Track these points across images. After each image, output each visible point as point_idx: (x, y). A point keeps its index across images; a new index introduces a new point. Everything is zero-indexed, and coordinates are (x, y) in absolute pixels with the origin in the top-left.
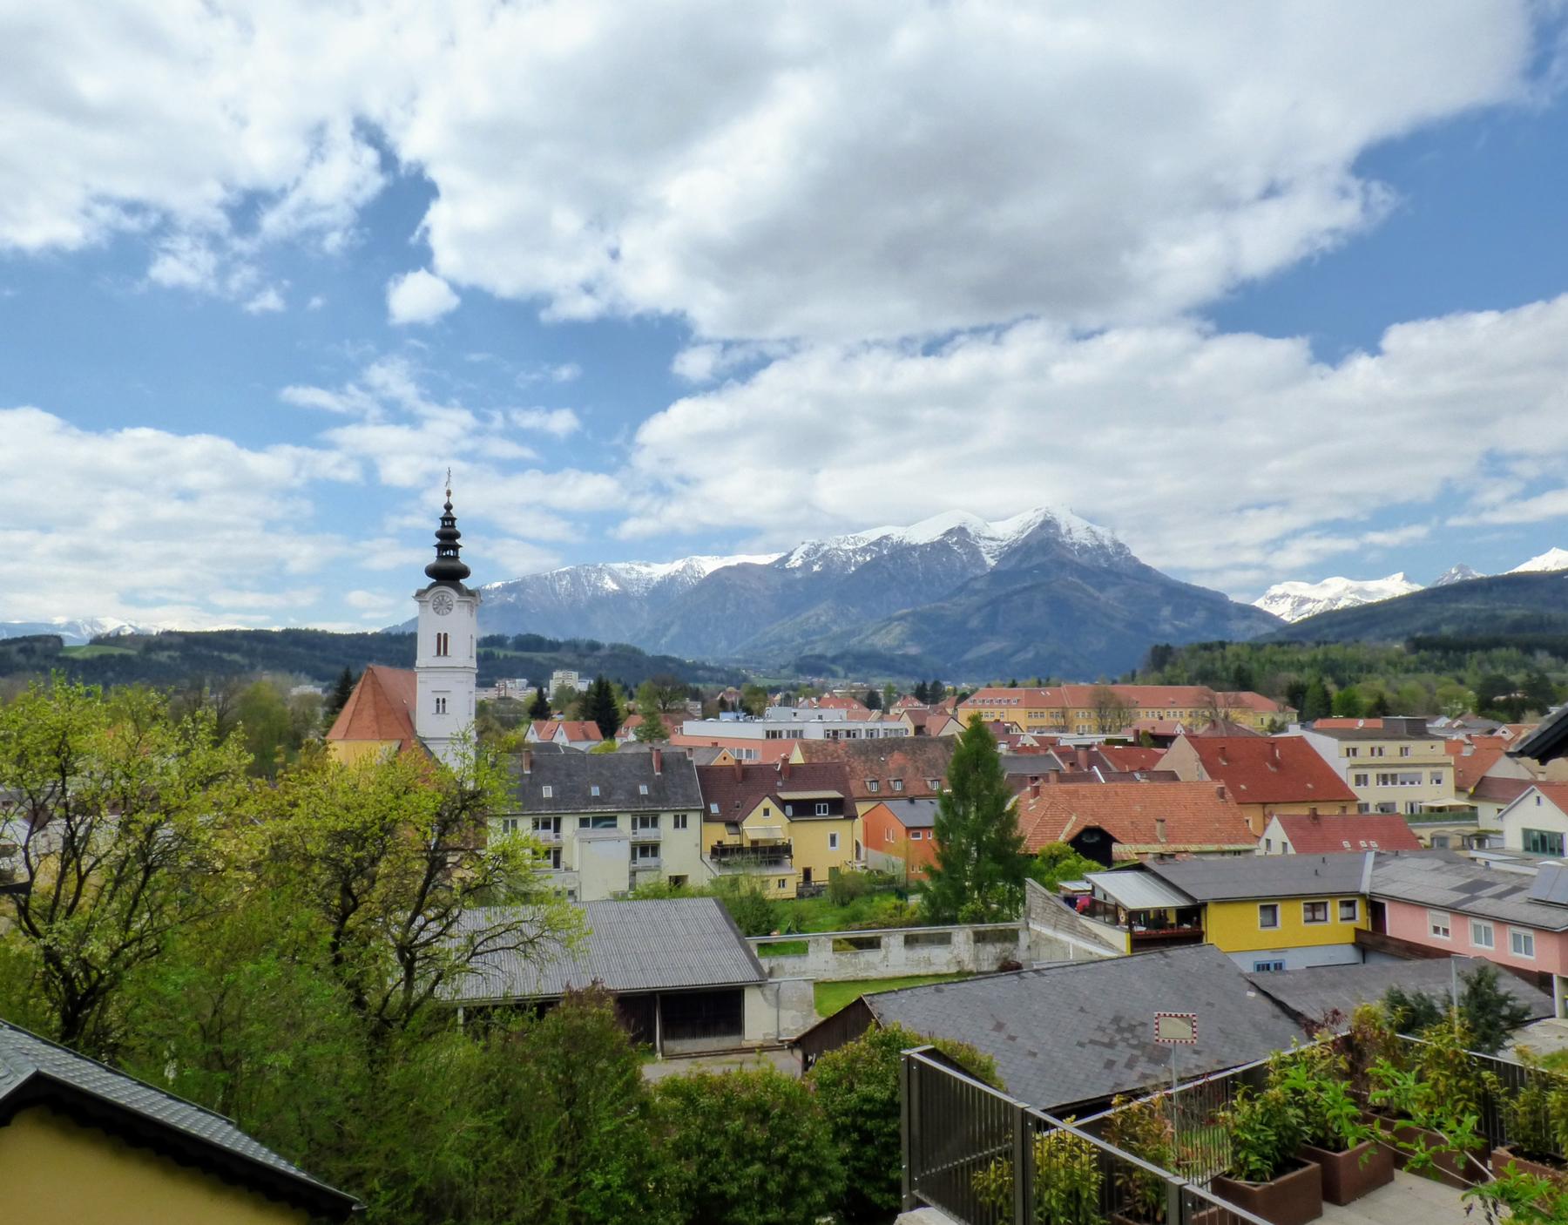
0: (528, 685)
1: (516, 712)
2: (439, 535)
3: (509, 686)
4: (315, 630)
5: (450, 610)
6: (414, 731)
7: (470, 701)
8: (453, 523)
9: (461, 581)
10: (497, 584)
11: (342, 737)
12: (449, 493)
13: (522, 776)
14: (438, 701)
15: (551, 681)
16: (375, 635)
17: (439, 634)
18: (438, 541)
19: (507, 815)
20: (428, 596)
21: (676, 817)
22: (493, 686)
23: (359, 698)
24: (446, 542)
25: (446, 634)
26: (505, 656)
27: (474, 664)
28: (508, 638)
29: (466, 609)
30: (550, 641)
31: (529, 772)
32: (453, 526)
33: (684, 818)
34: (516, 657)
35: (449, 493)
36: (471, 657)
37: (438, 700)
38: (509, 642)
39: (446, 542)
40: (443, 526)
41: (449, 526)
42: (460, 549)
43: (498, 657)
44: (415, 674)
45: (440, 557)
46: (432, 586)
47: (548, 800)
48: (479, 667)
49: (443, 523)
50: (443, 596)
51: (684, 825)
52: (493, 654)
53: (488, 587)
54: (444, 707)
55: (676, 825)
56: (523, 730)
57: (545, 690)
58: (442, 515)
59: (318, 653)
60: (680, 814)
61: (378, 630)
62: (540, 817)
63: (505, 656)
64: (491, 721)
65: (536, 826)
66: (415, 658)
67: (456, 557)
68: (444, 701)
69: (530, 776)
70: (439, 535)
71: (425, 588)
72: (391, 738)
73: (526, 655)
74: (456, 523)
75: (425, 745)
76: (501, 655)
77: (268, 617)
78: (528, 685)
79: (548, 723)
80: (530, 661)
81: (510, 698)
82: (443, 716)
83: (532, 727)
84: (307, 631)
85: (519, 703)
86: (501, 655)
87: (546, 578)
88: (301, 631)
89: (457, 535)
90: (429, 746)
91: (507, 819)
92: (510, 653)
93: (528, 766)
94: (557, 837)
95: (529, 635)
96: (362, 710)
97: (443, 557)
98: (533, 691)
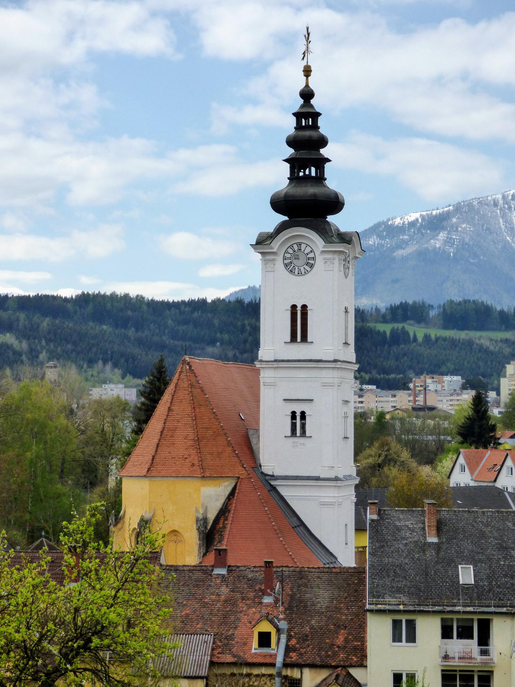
0: (464, 387)
1: (437, 431)
2: (291, 142)
3: (432, 387)
4: (126, 296)
5: (312, 266)
6: (256, 465)
7: (346, 417)
8: (315, 122)
9: (330, 218)
10: (413, 217)
11: (144, 472)
12: (307, 72)
13: (424, 546)
14: (293, 415)
15: (503, 380)
16: (217, 302)
17: (294, 307)
18: (290, 152)
19: (399, 612)
20: (276, 245)
21: (396, 624)
22: (405, 387)
23: (170, 409)
24: (304, 154)
25: (304, 307)
26: (427, 337)
27: (350, 354)
28: (431, 307)
29: (337, 262)
30: (502, 313)
31: (435, 540)
32: (315, 127)
33: (411, 625)
34: (445, 339)
35: (307, 72)
36: (346, 343)
37: (294, 414)
38: (432, 313)
39: (304, 154)
40: (299, 127)
41: (307, 127)
42: (327, 165)
43: (415, 339)
44: (257, 371)
45: (293, 178)
46: (282, 228)
47: (467, 588)
48: (358, 361)
49: (299, 122)
50: (299, 244)
51: (412, 638)
52: (405, 333)
53: (398, 221)
54: (303, 426)
55: (397, 638)
56: (446, 463)
57: (492, 395)
58: (296, 109)
59: (131, 332)
60: (404, 618)
61: (223, 294)
62: (455, 617)
63: (427, 337)
64: (395, 446)
65: (446, 633)
66: (256, 344)
67: (320, 179)
68: (303, 415)
69: (438, 547)
70: (291, 142)
71: (271, 229)
72: (219, 477)
73: (463, 335)
74: (321, 121)
75: (274, 488)
76: (420, 337)
77: (47, 276)
78: (464, 387)
79: (489, 453)
80: (470, 343)
81: (432, 409)
82: (302, 440)
83: (461, 460)
84: (113, 297)
85: (447, 417)
86: (420, 337)
87: (496, 204)
88: (104, 296)
89: (323, 142)
90: (279, 489)
91: (397, 617)
92: (434, 333)
93: (434, 532)
94: (484, 653)
95: (466, 302)
96: (175, 429)
97: (299, 178)
98: (468, 396)
